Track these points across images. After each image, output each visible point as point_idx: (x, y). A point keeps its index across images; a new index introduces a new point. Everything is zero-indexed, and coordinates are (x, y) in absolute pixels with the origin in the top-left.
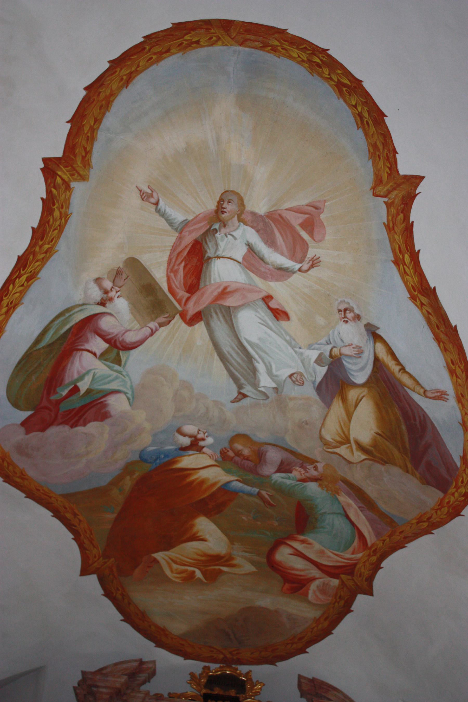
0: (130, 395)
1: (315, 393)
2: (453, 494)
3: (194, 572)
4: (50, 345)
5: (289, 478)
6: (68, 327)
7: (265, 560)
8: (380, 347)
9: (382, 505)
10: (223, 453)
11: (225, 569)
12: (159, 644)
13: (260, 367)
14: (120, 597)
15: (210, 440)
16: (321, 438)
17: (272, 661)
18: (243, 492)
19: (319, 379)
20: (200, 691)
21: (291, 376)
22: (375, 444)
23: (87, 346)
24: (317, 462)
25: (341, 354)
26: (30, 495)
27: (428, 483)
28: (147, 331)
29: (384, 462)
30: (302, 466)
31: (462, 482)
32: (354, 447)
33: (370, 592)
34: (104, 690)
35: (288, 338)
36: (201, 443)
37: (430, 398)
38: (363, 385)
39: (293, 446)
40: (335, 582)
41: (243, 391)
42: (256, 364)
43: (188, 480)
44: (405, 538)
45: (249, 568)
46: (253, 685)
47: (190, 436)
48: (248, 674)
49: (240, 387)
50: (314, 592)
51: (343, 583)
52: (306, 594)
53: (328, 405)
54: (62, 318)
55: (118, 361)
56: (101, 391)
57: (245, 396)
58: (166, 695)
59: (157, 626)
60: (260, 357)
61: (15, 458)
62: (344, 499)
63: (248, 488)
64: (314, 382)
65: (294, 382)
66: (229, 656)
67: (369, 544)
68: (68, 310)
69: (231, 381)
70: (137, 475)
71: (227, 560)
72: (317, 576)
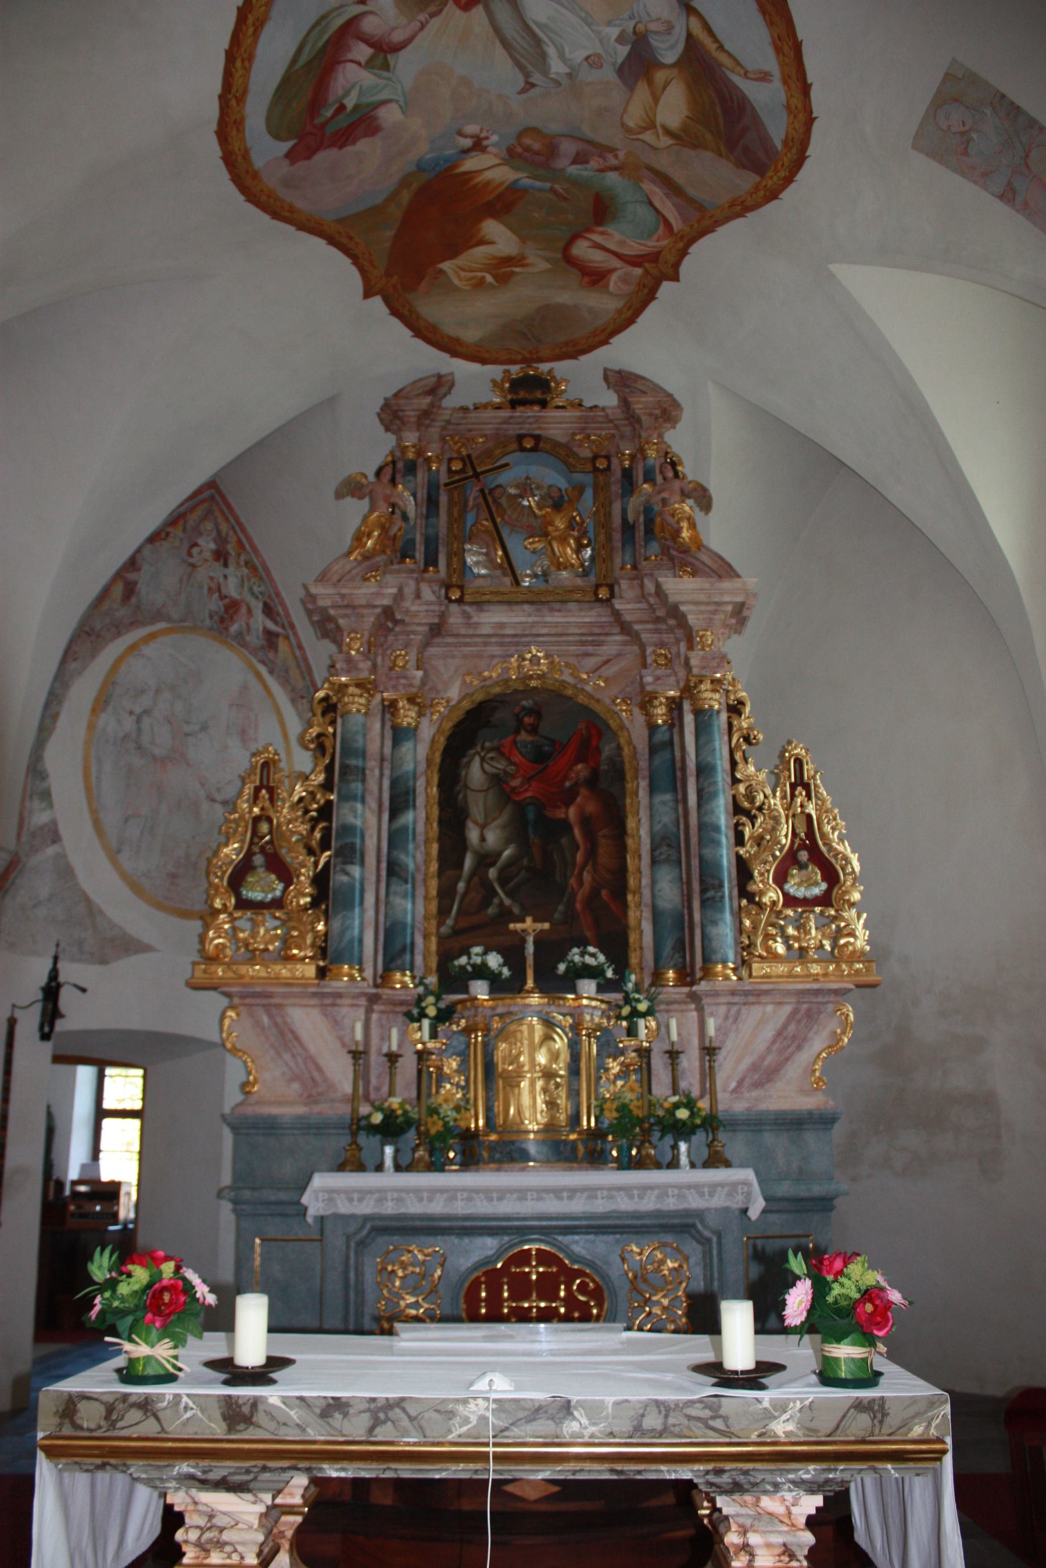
0: (402, 103)
1: (615, 75)
2: (771, 178)
3: (483, 278)
4: (309, 63)
5: (586, 169)
6: (326, 37)
7: (560, 256)
8: (694, 22)
9: (691, 192)
10: (510, 151)
11: (517, 270)
12: (455, 354)
13: (551, 51)
14: (406, 313)
15: (494, 138)
16: (623, 125)
17: (574, 355)
18: (533, 188)
19: (620, 60)
20: (505, 397)
21: (587, 59)
22: (685, 128)
23: (350, 56)
24: (617, 150)
25: (647, 30)
26: (301, 227)
27: (744, 167)
28: (416, 25)
29: (695, 147)
30: (600, 156)
31: (783, 165)
32: (660, 132)
33: (675, 278)
34: (412, 413)
35: (583, 14)
36: (485, 143)
37: (752, 79)
38: (675, 65)
39: (590, 134)
40: (638, 271)
41: (531, 80)
42: (546, 48)
43: (472, 183)
44: (715, 222)
45: (544, 265)
46: (558, 384)
47: (472, 137)
48: (550, 371)
49: (527, 75)
50: (615, 283)
51: (647, 272)
52: (607, 286)
53: (632, 89)
54: (319, 28)
55: (386, 67)
56: (368, 105)
57: (533, 85)
58: (471, 407)
59: (449, 337)
60: (550, 39)
61: (282, 193)
62: (648, 186)
63: (538, 184)
64: (614, 64)
65: (591, 65)
66: (527, 355)
67: (676, 230)
68: (323, 17)
69: (517, 70)
70: (415, 186)
71: (520, 260)
72: (618, 266)
